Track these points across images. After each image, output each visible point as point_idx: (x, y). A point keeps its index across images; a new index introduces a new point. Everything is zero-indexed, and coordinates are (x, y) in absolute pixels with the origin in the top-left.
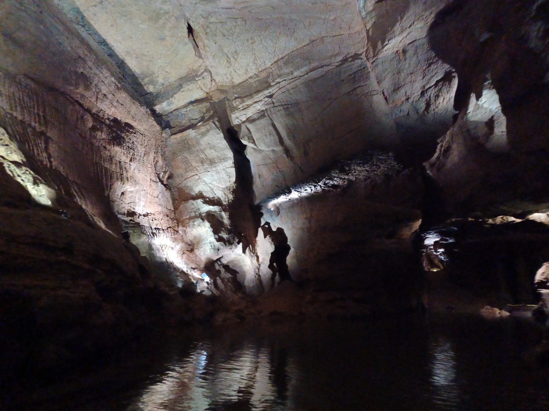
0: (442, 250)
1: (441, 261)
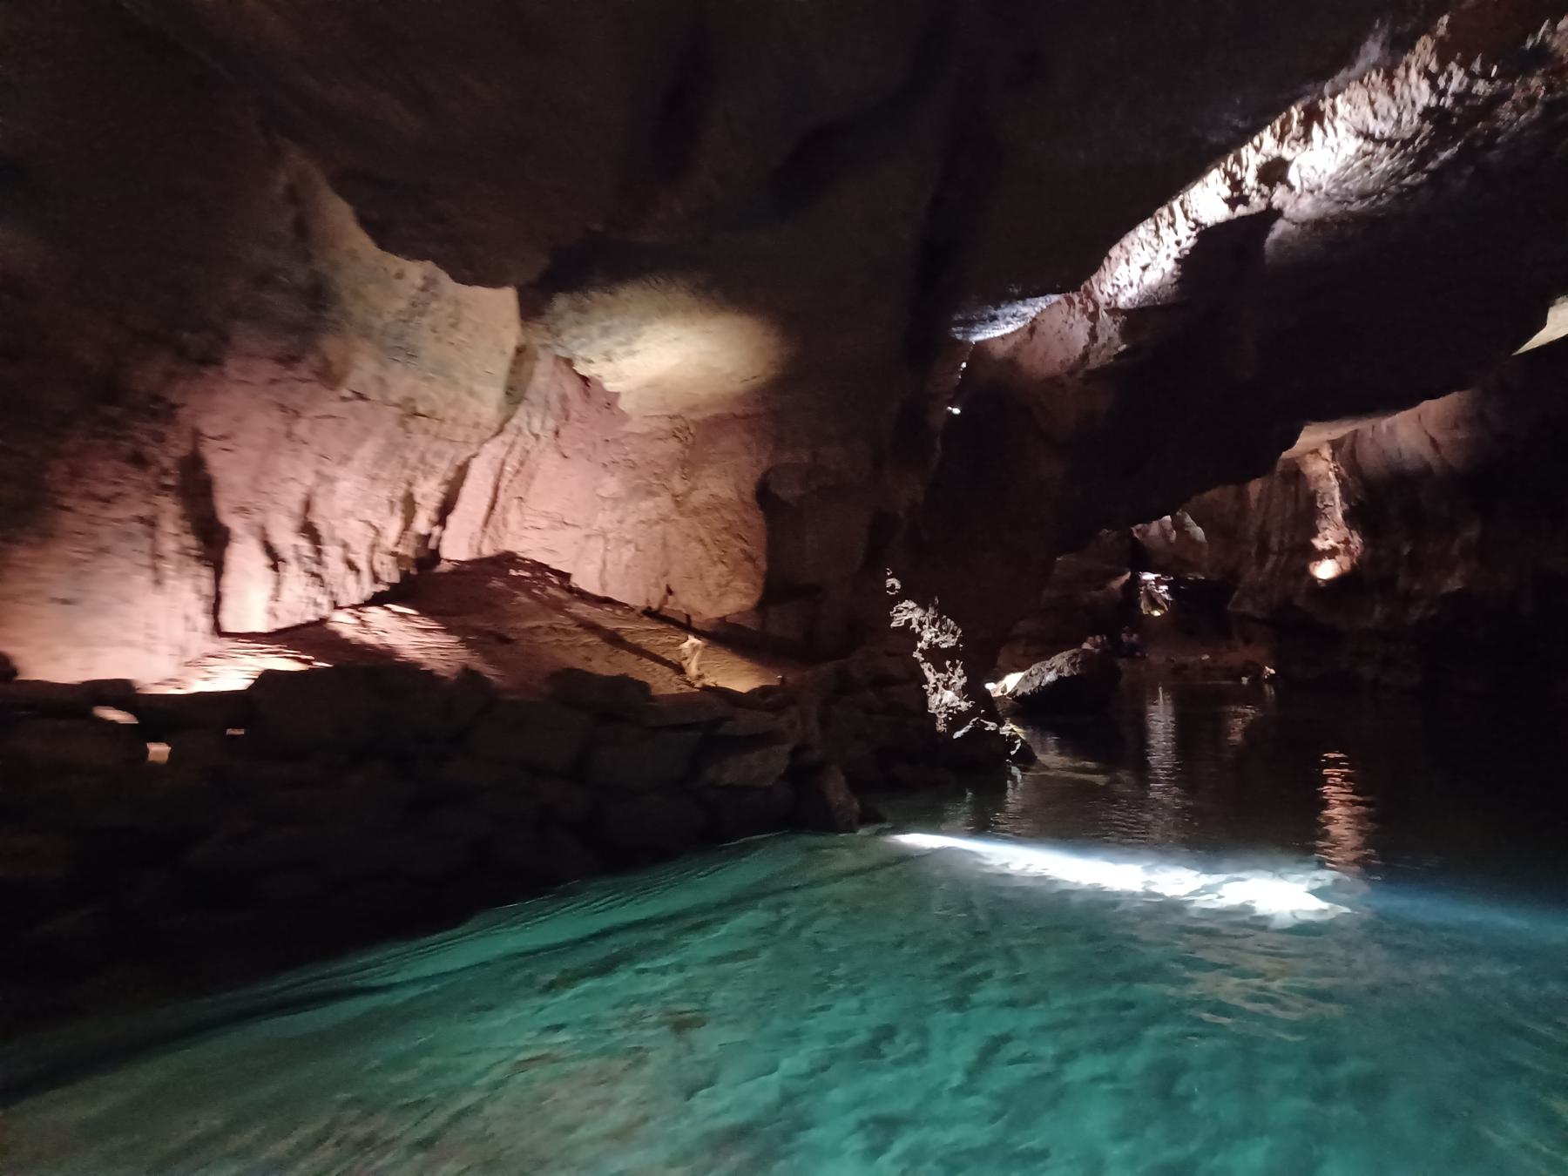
0: (1165, 588)
1: (1166, 601)
